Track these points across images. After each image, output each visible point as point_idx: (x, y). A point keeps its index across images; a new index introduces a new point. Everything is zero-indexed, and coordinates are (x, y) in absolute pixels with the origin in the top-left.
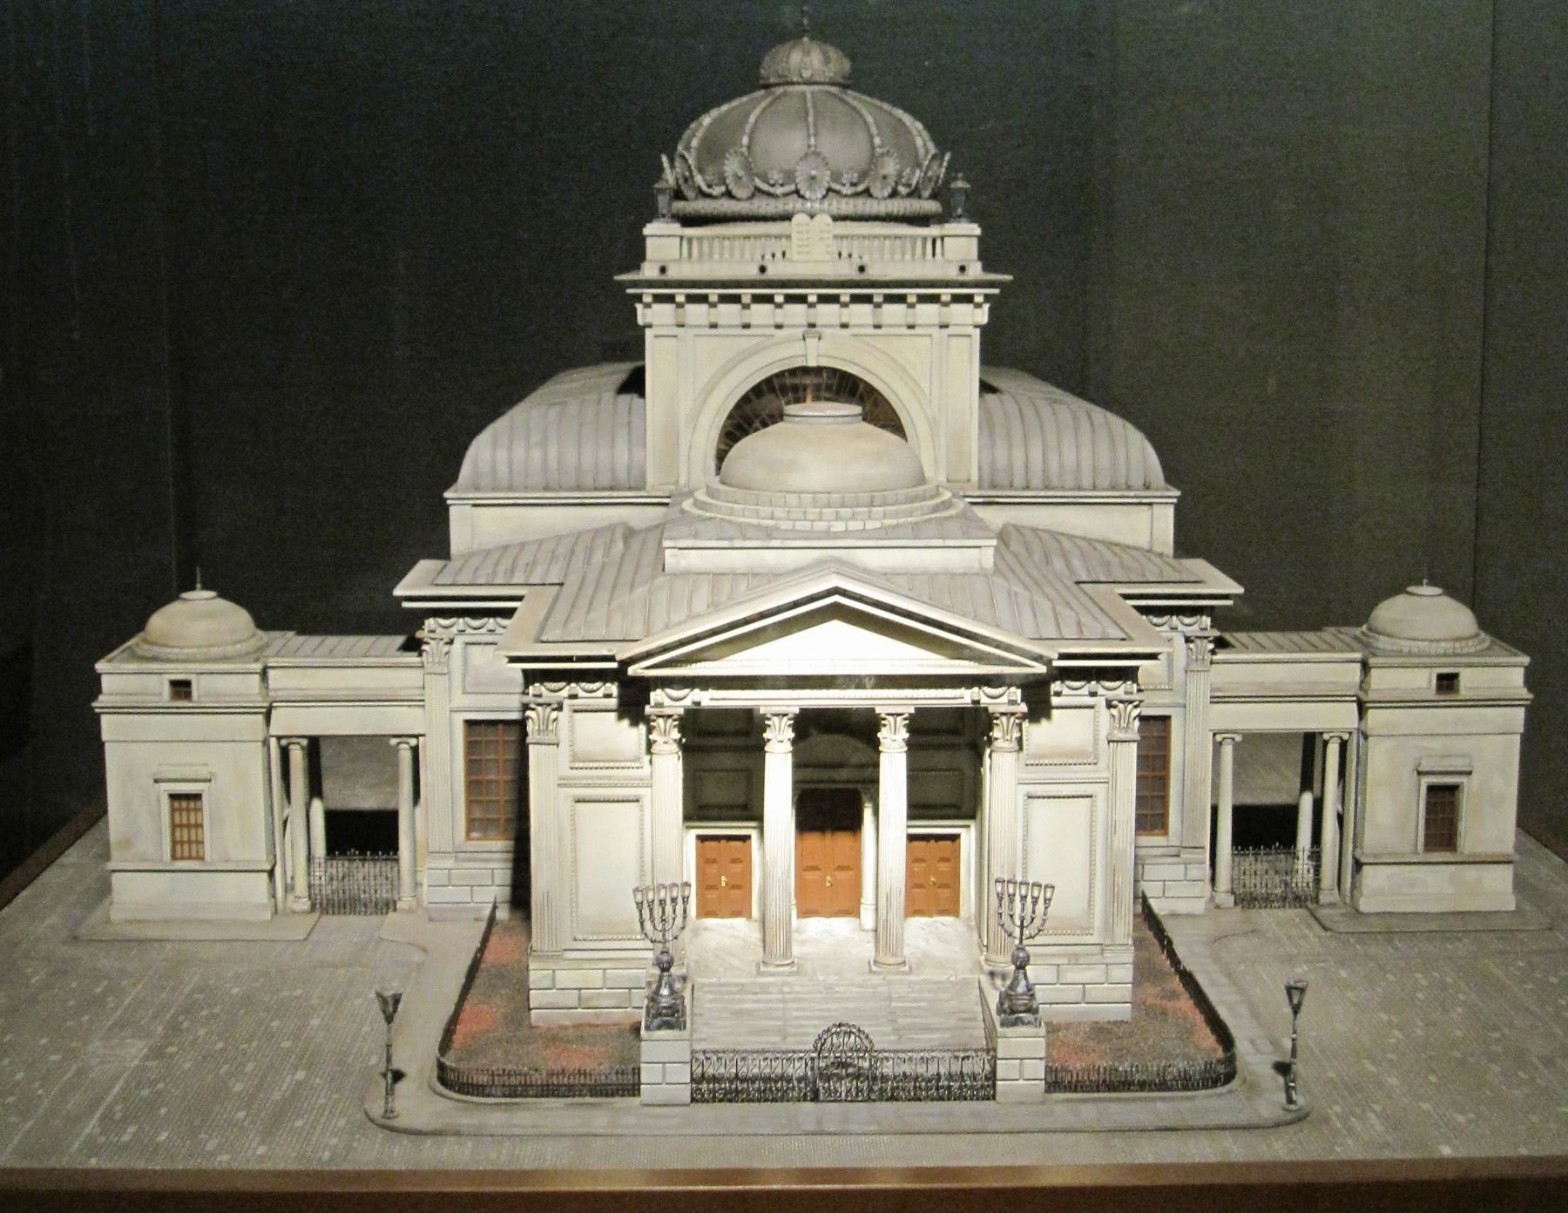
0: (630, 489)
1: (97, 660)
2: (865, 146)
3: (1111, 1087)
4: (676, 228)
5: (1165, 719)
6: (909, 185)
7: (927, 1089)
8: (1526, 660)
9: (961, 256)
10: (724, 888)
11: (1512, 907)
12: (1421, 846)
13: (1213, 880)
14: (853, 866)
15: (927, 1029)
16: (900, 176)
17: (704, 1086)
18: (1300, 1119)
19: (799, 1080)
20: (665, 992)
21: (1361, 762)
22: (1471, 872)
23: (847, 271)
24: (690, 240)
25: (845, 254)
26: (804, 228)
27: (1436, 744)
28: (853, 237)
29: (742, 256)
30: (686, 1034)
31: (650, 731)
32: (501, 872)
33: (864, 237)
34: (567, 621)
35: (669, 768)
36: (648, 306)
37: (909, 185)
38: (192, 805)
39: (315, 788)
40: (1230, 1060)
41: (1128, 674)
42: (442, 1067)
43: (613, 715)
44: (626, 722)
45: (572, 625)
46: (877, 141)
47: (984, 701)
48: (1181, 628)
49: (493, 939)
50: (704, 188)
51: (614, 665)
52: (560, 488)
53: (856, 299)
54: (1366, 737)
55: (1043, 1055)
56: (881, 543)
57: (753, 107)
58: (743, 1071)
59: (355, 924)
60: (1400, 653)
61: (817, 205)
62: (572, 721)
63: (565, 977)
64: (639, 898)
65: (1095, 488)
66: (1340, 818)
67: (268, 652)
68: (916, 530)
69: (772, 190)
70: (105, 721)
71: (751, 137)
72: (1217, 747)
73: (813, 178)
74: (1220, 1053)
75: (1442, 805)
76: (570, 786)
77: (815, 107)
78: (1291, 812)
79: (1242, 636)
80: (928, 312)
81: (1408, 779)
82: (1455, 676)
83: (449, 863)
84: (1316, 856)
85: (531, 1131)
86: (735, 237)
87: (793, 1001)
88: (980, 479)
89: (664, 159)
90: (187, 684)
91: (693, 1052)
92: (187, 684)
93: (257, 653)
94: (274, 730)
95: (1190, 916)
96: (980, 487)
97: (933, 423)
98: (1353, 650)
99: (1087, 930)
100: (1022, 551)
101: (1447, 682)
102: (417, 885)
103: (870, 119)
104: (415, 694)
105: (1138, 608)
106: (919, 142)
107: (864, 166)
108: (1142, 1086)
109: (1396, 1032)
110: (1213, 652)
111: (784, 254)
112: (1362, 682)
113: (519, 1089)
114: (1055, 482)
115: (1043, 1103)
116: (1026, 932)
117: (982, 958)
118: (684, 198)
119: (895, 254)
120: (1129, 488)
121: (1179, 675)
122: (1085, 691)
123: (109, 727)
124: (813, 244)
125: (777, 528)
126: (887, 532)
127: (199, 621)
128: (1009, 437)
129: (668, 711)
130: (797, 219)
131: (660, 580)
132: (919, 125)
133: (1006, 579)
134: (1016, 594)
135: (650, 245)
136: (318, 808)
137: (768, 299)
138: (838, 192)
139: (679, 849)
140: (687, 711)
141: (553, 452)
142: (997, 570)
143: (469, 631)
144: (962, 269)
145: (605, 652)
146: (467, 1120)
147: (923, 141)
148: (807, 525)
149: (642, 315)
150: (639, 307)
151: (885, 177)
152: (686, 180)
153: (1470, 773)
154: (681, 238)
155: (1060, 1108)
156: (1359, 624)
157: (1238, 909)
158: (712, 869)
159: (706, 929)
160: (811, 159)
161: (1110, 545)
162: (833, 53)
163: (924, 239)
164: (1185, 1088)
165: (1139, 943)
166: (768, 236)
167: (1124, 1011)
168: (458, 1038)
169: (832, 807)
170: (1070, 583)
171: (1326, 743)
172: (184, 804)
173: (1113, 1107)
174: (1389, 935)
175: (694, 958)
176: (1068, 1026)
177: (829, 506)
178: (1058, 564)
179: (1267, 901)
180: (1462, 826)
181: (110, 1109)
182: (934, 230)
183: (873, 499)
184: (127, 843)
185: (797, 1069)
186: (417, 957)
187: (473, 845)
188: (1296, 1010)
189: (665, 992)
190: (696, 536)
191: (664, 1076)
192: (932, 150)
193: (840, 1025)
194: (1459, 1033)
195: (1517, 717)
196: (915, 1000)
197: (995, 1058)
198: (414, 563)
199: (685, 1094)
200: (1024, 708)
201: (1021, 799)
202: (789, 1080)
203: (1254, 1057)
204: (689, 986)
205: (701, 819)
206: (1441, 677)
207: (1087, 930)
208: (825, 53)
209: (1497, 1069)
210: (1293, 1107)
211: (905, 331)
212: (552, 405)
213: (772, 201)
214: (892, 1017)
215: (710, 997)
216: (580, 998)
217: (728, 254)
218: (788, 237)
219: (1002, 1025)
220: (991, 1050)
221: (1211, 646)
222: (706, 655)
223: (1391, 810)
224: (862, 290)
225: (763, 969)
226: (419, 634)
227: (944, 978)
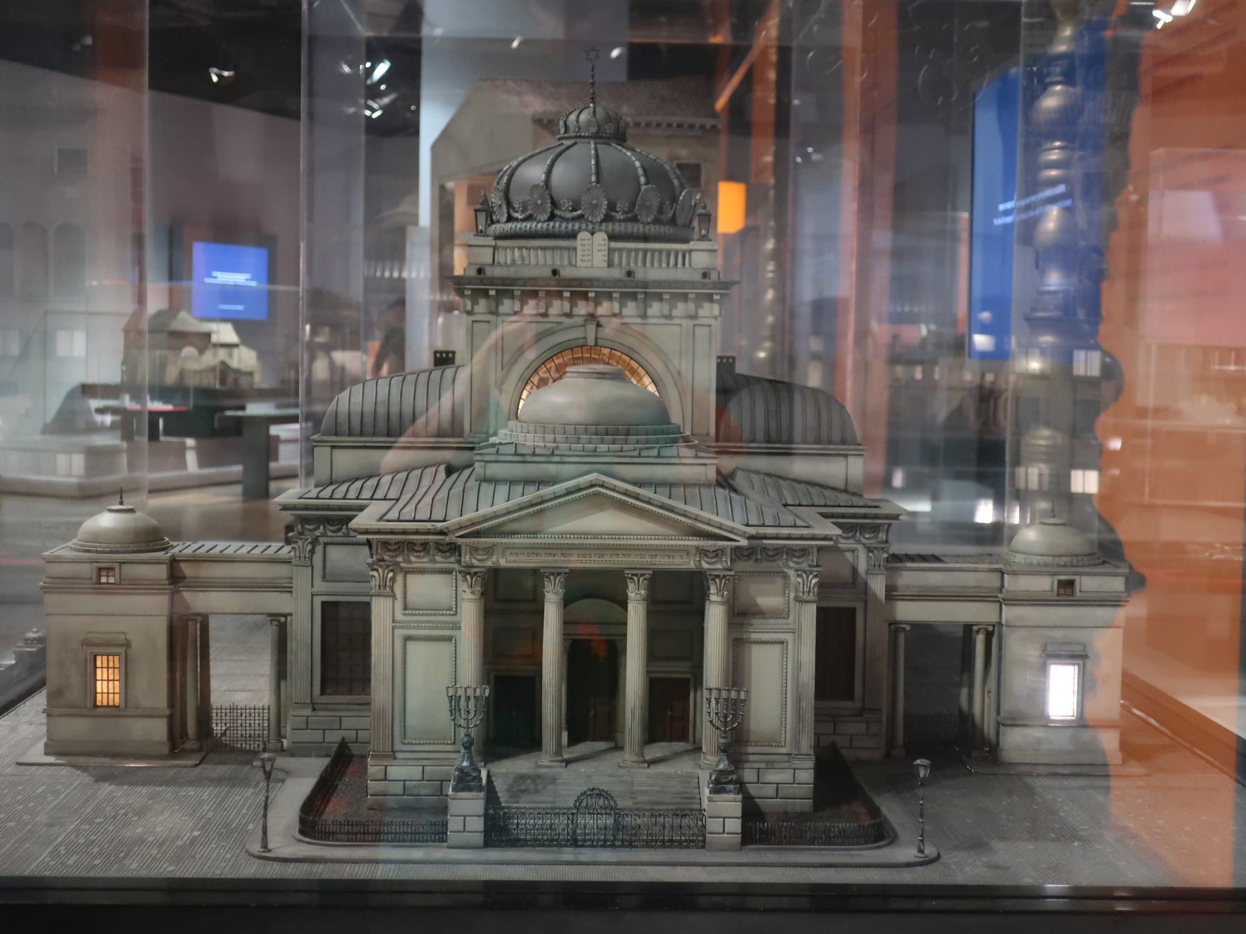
9: (704, 265)
48: (864, 541)
61: (597, 226)
96: (717, 440)
104: (285, 582)
107: (850, 489)
130: (580, 236)
169: (593, 665)
181: (56, 848)
206: (1061, 583)
214: (633, 795)
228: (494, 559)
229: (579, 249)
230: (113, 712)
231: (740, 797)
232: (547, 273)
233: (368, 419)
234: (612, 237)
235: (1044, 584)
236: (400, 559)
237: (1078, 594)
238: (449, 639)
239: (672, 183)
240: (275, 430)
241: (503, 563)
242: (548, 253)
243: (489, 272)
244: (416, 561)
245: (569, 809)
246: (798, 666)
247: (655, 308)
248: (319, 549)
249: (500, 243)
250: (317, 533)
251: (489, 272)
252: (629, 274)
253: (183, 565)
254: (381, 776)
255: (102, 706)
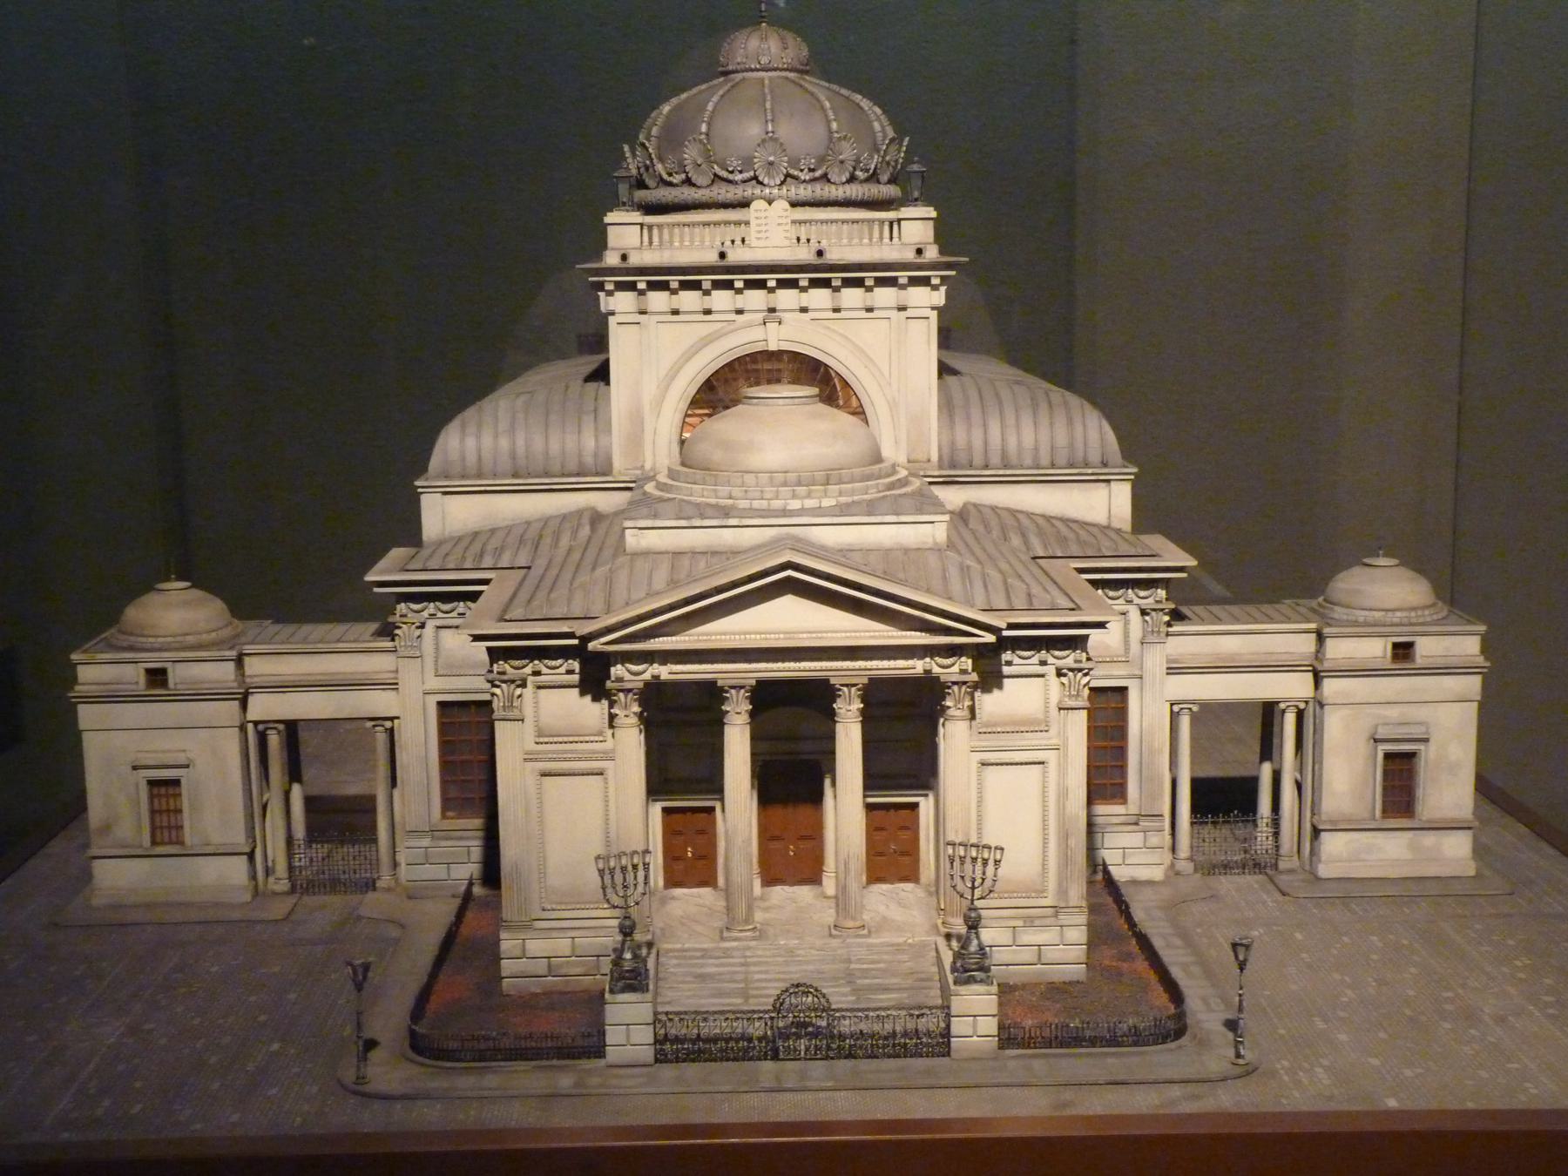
0: (597, 474)
1: (75, 648)
2: (821, 131)
3: (1062, 1045)
4: (636, 217)
5: (1123, 691)
6: (867, 171)
7: (884, 1047)
8: (1482, 628)
9: (917, 240)
10: (691, 856)
11: (1472, 873)
12: (1378, 813)
13: (1173, 849)
14: (815, 835)
15: (886, 989)
16: (858, 161)
17: (667, 1046)
18: (1248, 1073)
19: (760, 1039)
20: (628, 956)
21: (1318, 730)
22: (1429, 839)
23: (805, 255)
24: (650, 227)
25: (803, 240)
26: (763, 214)
27: (1393, 713)
28: (810, 222)
29: (702, 242)
30: (649, 996)
31: (611, 706)
32: (476, 849)
33: (822, 222)
34: (529, 601)
35: (630, 744)
36: (610, 293)
37: (867, 171)
38: (171, 791)
39: (294, 773)
40: (1180, 1016)
41: (1077, 643)
42: (413, 1035)
43: (576, 691)
44: (588, 698)
45: (535, 603)
46: (834, 126)
47: (936, 670)
48: (1137, 601)
49: (469, 915)
50: (665, 176)
51: (576, 642)
52: (529, 475)
53: (815, 283)
54: (1322, 705)
55: (995, 1012)
56: (836, 520)
57: (712, 96)
58: (704, 1032)
59: (335, 903)
60: (1356, 624)
61: (776, 191)
62: (437, 638)
63: (536, 946)
64: (601, 866)
65: (1053, 466)
66: (1299, 786)
67: (243, 639)
68: (871, 508)
69: (731, 177)
70: (83, 710)
71: (709, 124)
72: (1174, 717)
73: (771, 164)
74: (1172, 1009)
75: (1399, 776)
76: (536, 760)
77: (772, 91)
78: (1251, 784)
79: (1199, 609)
80: (885, 296)
81: (1362, 747)
82: (1410, 645)
83: (426, 842)
84: (1276, 822)
85: (498, 1093)
86: (694, 224)
87: (755, 964)
88: (940, 457)
89: (626, 148)
90: (163, 672)
91: (656, 1014)
92: (163, 672)
93: (230, 642)
94: (251, 716)
95: (1150, 883)
96: (941, 467)
97: (893, 406)
98: (1309, 621)
99: (1041, 892)
100: (981, 529)
101: (1403, 651)
102: (395, 865)
103: (827, 104)
105: (1091, 582)
106: (876, 125)
107: (822, 151)
108: (1093, 1042)
109: (1349, 992)
110: (1169, 624)
111: (743, 241)
112: (1318, 652)
113: (489, 1053)
114: (1014, 461)
115: (995, 1059)
116: (977, 893)
117: (940, 922)
118: (647, 187)
119: (852, 240)
120: (1087, 465)
121: (1135, 646)
122: (1035, 660)
123: (87, 715)
124: (771, 231)
125: (733, 507)
126: (843, 510)
127: (176, 612)
128: (968, 417)
129: (629, 686)
130: (754, 205)
131: (621, 559)
132: (878, 110)
133: (960, 554)
134: (968, 567)
135: (612, 233)
136: (297, 792)
137: (728, 285)
138: (796, 178)
139: (642, 824)
140: (647, 684)
141: (520, 442)
142: (951, 545)
143: (440, 615)
144: (919, 252)
145: (565, 629)
146: (437, 1083)
147: (880, 124)
148: (764, 504)
149: (606, 303)
150: (602, 294)
151: (842, 162)
152: (647, 168)
153: (1426, 740)
154: (642, 225)
155: (1012, 1064)
156: (1314, 596)
157: (1198, 875)
158: (679, 840)
159: (673, 898)
160: (769, 145)
161: (1066, 521)
162: (790, 38)
163: (882, 222)
164: (1135, 1044)
165: (1093, 909)
166: (727, 223)
167: (1078, 971)
168: (433, 1005)
169: (791, 781)
170: (1026, 558)
171: (1284, 711)
172: (163, 790)
173: (1064, 1062)
174: (1345, 899)
175: (661, 925)
176: (1024, 987)
177: (785, 484)
178: (1016, 541)
179: (1226, 867)
180: (1419, 793)
182: (891, 215)
183: (828, 477)
184: (106, 829)
185: (757, 1029)
186: (394, 932)
187: (447, 824)
188: (1242, 966)
189: (628, 956)
190: (655, 516)
191: (628, 1036)
192: (891, 133)
193: (798, 986)
194: (1411, 993)
195: (1473, 684)
196: (873, 962)
197: (948, 1016)
198: (386, 550)
199: (648, 1054)
200: (974, 677)
201: (974, 766)
202: (750, 1040)
203: (1205, 1011)
204: (654, 951)
205: (667, 793)
206: (1396, 646)
207: (1041, 892)
208: (782, 39)
209: (1447, 1026)
210: (1241, 1061)
211: (864, 314)
212: (518, 395)
213: (731, 188)
214: (850, 978)
215: (675, 962)
216: (549, 966)
217: (689, 241)
218: (747, 223)
219: (955, 983)
220: (946, 1008)
221: (1167, 618)
222: (666, 630)
223: (1347, 776)
224: (822, 274)
225: (726, 934)
226: (391, 619)
227: (901, 940)
229: (753, 222)
239: (872, 128)
245: (766, 1012)
246: (1063, 794)
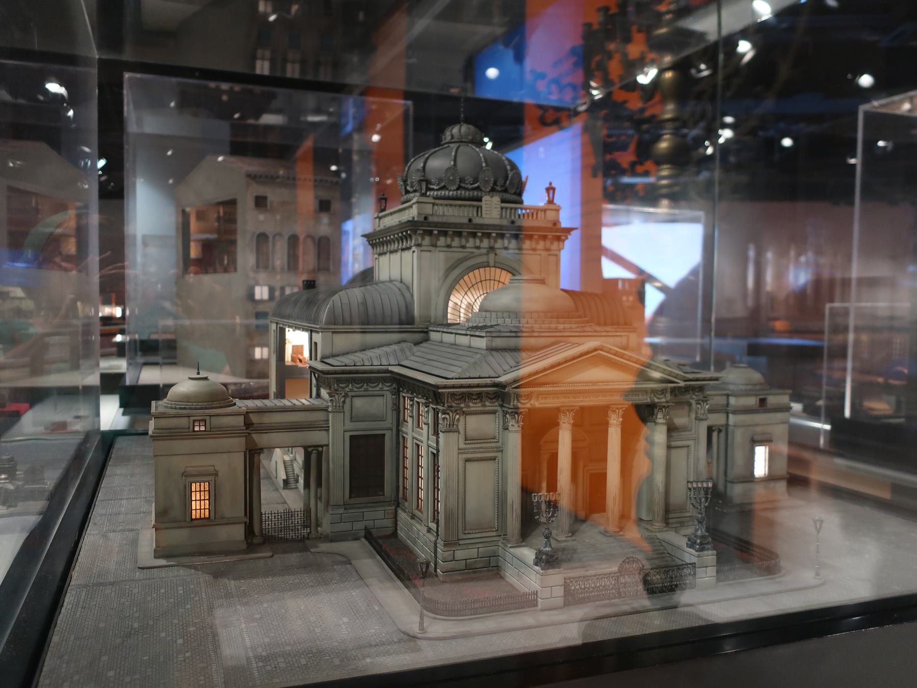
101: (763, 401)
187: (353, 501)
228: (532, 402)
230: (204, 522)
231: (715, 552)
232: (466, 221)
233: (347, 315)
234: (503, 201)
235: (752, 401)
236: (462, 405)
237: (769, 406)
238: (494, 459)
240: (47, 339)
241: (537, 405)
242: (466, 209)
243: (431, 219)
244: (475, 406)
246: (697, 460)
247: (527, 244)
248: (348, 400)
249: (437, 201)
250: (347, 389)
251: (431, 219)
252: (513, 222)
253: (251, 415)
254: (451, 558)
255: (196, 519)
